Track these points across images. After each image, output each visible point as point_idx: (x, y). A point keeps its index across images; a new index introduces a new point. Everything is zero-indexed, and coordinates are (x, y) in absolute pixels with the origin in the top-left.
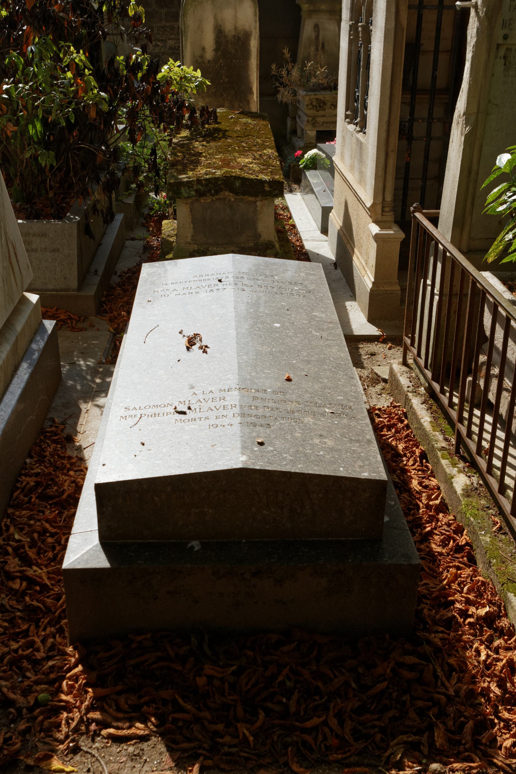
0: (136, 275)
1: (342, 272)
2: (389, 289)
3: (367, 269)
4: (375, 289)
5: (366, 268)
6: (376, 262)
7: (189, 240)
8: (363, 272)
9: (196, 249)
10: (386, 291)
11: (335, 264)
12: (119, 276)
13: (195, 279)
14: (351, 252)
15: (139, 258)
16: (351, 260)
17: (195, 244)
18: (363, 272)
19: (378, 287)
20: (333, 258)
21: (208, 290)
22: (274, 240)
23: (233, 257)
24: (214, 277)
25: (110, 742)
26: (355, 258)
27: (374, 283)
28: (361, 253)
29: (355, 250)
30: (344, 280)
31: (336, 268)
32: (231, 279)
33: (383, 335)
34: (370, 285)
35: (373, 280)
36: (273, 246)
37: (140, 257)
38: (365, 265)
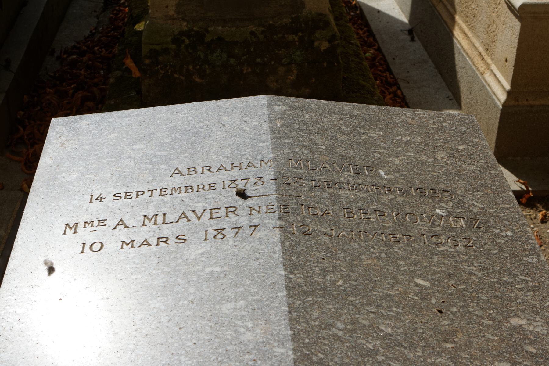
0: (37, 147)
1: (426, 48)
2: (537, 103)
3: (489, 61)
4: (512, 103)
5: (486, 57)
6: (518, 56)
7: (171, 13)
8: (481, 66)
9: (185, 29)
10: (532, 106)
11: (410, 32)
12: (58, 58)
13: (178, 181)
14: (448, 20)
15: (96, 20)
16: (450, 36)
17: (183, 19)
18: (481, 66)
19: (517, 100)
20: (404, 18)
21: (211, 232)
22: (328, 12)
23: (270, 106)
24: (226, 175)
25: (174, 8)
26: (457, 33)
27: (509, 93)
28: (472, 28)
29: (457, 18)
30: (430, 62)
31: (413, 39)
32: (270, 188)
33: (528, 192)
34: (503, 97)
35: (508, 87)
36: (327, 24)
37: (98, 17)
38: (483, 53)
